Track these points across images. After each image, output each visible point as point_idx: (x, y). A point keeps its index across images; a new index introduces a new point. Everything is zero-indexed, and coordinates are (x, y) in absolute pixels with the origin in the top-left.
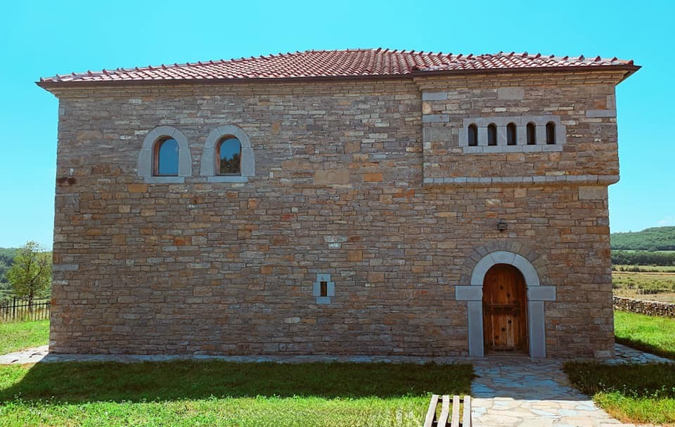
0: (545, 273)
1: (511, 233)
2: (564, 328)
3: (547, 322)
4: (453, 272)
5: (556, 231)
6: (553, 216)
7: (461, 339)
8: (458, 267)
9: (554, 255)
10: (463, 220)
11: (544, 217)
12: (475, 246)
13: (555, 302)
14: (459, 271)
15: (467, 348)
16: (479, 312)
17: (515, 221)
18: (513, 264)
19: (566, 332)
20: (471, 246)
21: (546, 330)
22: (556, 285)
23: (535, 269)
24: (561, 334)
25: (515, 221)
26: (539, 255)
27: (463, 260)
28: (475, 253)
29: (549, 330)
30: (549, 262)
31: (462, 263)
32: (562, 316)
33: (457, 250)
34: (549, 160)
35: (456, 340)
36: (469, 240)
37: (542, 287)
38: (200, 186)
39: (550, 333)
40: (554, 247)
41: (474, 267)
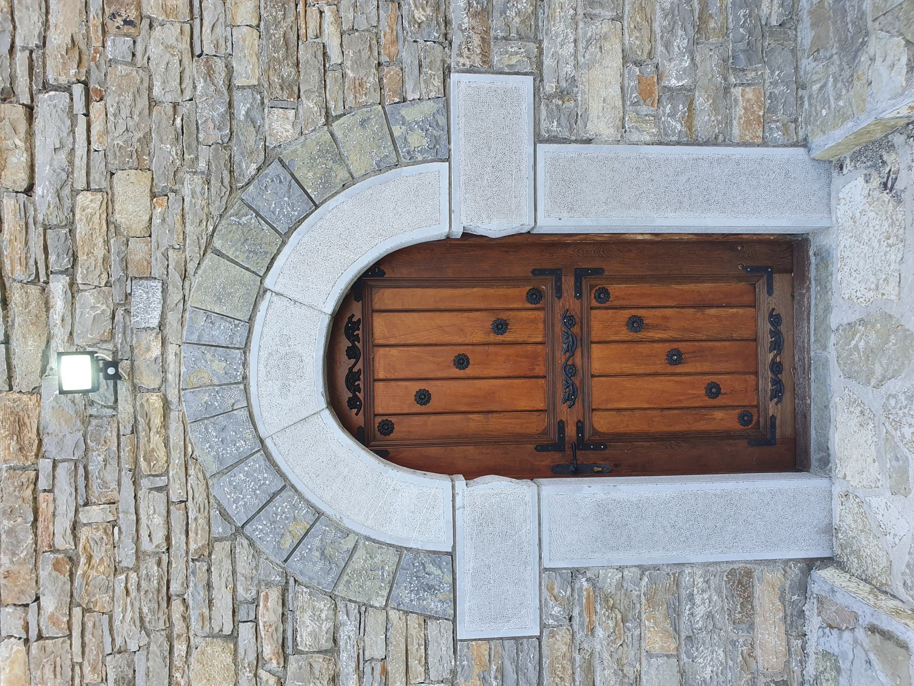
0: (374, 125)
1: (135, 321)
2: (680, 42)
3: (650, 131)
4: (376, 650)
5: (118, 46)
6: (21, 58)
7: (747, 600)
8: (348, 630)
9: (270, 66)
10: (49, 604)
11: (30, 110)
12: (218, 529)
13: (539, 78)
14: (375, 621)
15: (795, 572)
16: (602, 509)
17: (58, 286)
18: (330, 307)
19: (701, 27)
20: (220, 551)
21: (695, 143)
22: (447, 72)
23: (353, 180)
24: (710, 63)
25: (58, 286)
26: (269, 156)
27: (301, 597)
28: (257, 529)
29: (689, 119)
30: (310, 104)
31: (323, 606)
32: (614, 47)
33: (246, 631)
34: (593, 410)
35: (752, 626)
36: (178, 566)
37: (459, 146)
38: (144, 533)
39: (705, 121)
40: (219, 65)
41: (347, 533)
